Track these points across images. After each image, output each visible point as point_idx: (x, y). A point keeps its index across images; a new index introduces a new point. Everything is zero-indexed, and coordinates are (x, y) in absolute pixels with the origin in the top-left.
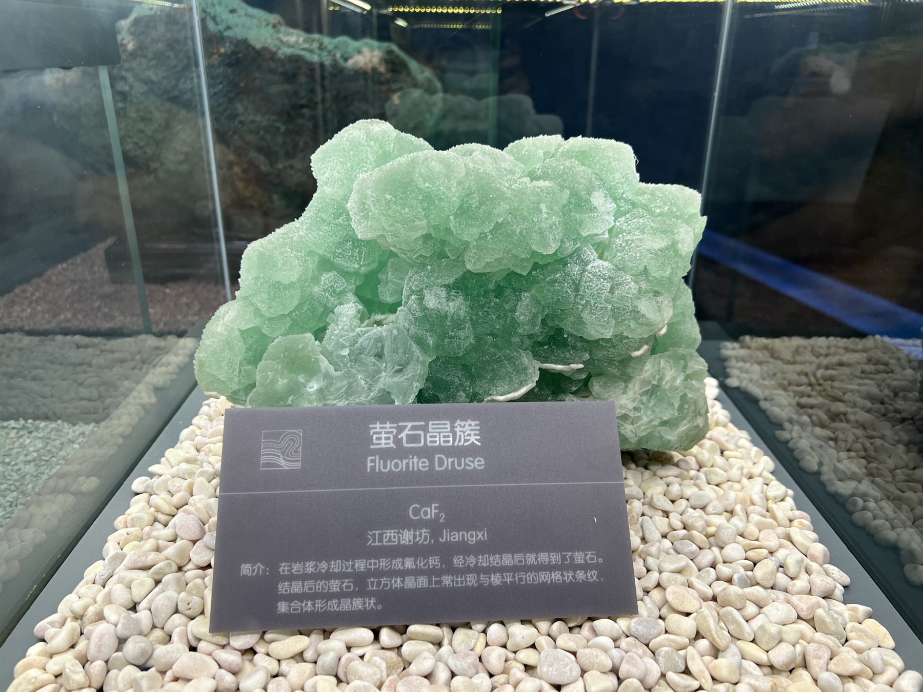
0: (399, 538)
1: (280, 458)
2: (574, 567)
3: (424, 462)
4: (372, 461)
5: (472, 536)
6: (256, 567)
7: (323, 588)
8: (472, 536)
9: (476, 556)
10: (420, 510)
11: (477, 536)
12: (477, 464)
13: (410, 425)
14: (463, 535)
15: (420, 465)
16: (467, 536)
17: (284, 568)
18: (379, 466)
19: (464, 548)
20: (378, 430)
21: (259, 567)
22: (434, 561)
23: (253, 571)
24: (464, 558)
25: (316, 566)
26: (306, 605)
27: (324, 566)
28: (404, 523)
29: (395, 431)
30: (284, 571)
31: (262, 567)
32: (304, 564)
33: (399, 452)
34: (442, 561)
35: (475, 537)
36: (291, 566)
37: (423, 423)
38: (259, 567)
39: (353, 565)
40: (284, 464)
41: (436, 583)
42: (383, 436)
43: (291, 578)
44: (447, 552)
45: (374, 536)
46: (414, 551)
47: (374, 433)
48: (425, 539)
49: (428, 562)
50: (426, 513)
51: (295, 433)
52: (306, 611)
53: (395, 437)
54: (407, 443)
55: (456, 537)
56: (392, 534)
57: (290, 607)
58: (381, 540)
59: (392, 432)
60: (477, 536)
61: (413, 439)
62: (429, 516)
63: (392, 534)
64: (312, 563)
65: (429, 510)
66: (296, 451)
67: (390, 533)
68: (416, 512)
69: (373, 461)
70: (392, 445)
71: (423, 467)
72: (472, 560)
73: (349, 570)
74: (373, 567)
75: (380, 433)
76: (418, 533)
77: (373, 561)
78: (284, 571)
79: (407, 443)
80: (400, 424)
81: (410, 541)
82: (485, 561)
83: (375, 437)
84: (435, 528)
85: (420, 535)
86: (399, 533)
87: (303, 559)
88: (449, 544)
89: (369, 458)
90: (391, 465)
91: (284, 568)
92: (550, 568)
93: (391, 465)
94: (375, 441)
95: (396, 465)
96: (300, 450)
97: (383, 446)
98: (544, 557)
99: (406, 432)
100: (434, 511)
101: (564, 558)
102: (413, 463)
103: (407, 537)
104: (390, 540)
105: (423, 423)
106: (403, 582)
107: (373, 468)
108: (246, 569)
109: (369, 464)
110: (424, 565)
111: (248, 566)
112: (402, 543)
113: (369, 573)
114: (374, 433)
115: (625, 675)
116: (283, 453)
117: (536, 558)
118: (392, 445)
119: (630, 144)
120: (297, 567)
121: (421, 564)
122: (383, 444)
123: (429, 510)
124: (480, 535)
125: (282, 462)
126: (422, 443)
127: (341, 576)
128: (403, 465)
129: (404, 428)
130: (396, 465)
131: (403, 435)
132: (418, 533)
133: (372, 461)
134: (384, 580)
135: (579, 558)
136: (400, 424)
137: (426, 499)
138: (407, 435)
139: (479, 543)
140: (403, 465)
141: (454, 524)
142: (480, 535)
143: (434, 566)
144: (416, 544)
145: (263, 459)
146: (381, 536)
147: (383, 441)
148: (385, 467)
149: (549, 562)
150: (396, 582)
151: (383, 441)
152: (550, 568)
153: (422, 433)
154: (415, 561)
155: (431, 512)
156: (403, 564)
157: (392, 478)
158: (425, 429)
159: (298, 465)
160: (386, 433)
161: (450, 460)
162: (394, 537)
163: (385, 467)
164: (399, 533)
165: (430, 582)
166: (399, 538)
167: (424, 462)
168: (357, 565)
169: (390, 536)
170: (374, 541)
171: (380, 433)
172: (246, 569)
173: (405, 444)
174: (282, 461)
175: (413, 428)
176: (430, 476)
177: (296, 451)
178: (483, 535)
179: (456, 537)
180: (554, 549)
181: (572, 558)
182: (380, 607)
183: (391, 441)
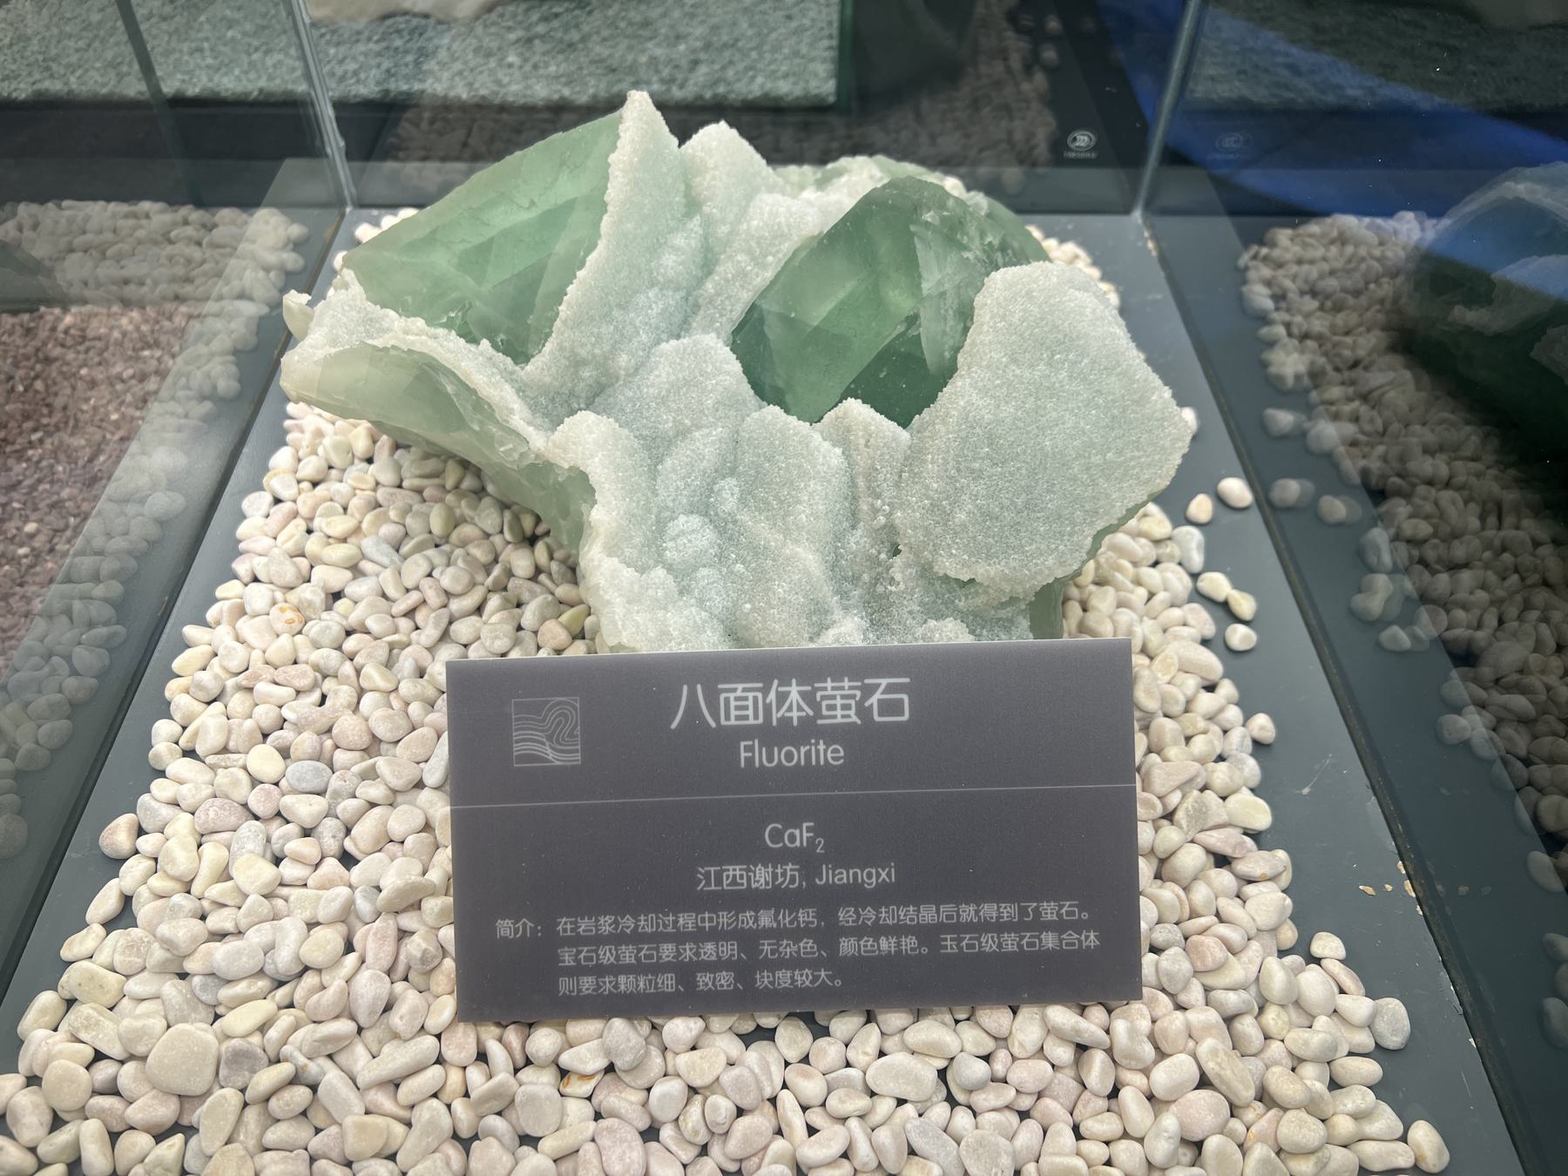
0: (749, 878)
1: (546, 747)
2: (1039, 926)
3: (836, 751)
4: (747, 749)
5: (870, 876)
8: (870, 876)
9: (797, 942)
11: (878, 875)
12: (828, 754)
13: (884, 682)
14: (855, 875)
15: (829, 755)
16: (862, 876)
17: (564, 925)
18: (760, 757)
19: (855, 895)
20: (829, 692)
21: (524, 925)
22: (806, 916)
24: (856, 912)
25: (616, 923)
26: (1087, 937)
27: (628, 922)
28: (754, 853)
29: (858, 693)
30: (565, 930)
32: (597, 921)
33: (773, 734)
34: (819, 916)
36: (575, 923)
38: (524, 925)
39: (676, 922)
40: (552, 756)
42: (839, 702)
44: (827, 901)
45: (707, 875)
46: (773, 898)
47: (823, 698)
48: (793, 880)
49: (796, 918)
50: (792, 838)
52: (1088, 947)
53: (860, 705)
54: (902, 714)
55: (843, 877)
57: (1061, 941)
58: (719, 882)
59: (853, 697)
60: (878, 875)
62: (798, 843)
64: (609, 919)
65: (797, 832)
66: (571, 735)
67: (733, 870)
68: (777, 836)
69: (749, 749)
70: (854, 719)
72: (869, 914)
73: (670, 930)
75: (834, 697)
76: (779, 871)
78: (565, 930)
79: (880, 715)
80: (867, 681)
81: (767, 883)
82: (887, 916)
83: (824, 703)
84: (807, 861)
85: (784, 874)
86: (748, 870)
87: (595, 911)
88: (829, 888)
89: (743, 744)
90: (779, 756)
91: (564, 925)
92: (999, 927)
93: (779, 756)
94: (825, 712)
95: (789, 756)
96: (578, 731)
97: (839, 720)
98: (989, 910)
99: (878, 696)
100: (805, 835)
101: (1023, 912)
102: (818, 751)
103: (762, 877)
104: (734, 882)
107: (750, 761)
108: (505, 928)
109: (743, 755)
110: (791, 922)
111: (508, 923)
112: (754, 886)
113: (941, 928)
114: (823, 698)
115: (690, 1148)
116: (550, 738)
117: (977, 912)
118: (854, 719)
120: (585, 925)
121: (786, 919)
122: (839, 717)
123: (797, 832)
124: (884, 875)
125: (551, 755)
126: (906, 717)
128: (799, 755)
129: (878, 685)
130: (789, 756)
131: (873, 700)
132: (779, 871)
133: (747, 749)
135: (1049, 911)
136: (867, 681)
138: (880, 701)
139: (882, 886)
140: (799, 755)
141: (840, 857)
142: (884, 875)
144: (776, 888)
145: (518, 749)
146: (719, 876)
147: (839, 712)
148: (770, 760)
149: (998, 918)
151: (839, 712)
152: (999, 927)
154: (776, 915)
155: (801, 835)
156: (756, 920)
159: (577, 758)
160: (843, 697)
161: (803, 750)
162: (741, 877)
163: (770, 760)
164: (748, 870)
166: (749, 878)
167: (836, 751)
168: (681, 921)
170: (708, 883)
171: (834, 697)
172: (505, 928)
173: (877, 718)
174: (549, 751)
175: (890, 689)
177: (571, 735)
178: (889, 875)
179: (843, 877)
180: (1010, 899)
181: (1036, 911)
183: (852, 712)
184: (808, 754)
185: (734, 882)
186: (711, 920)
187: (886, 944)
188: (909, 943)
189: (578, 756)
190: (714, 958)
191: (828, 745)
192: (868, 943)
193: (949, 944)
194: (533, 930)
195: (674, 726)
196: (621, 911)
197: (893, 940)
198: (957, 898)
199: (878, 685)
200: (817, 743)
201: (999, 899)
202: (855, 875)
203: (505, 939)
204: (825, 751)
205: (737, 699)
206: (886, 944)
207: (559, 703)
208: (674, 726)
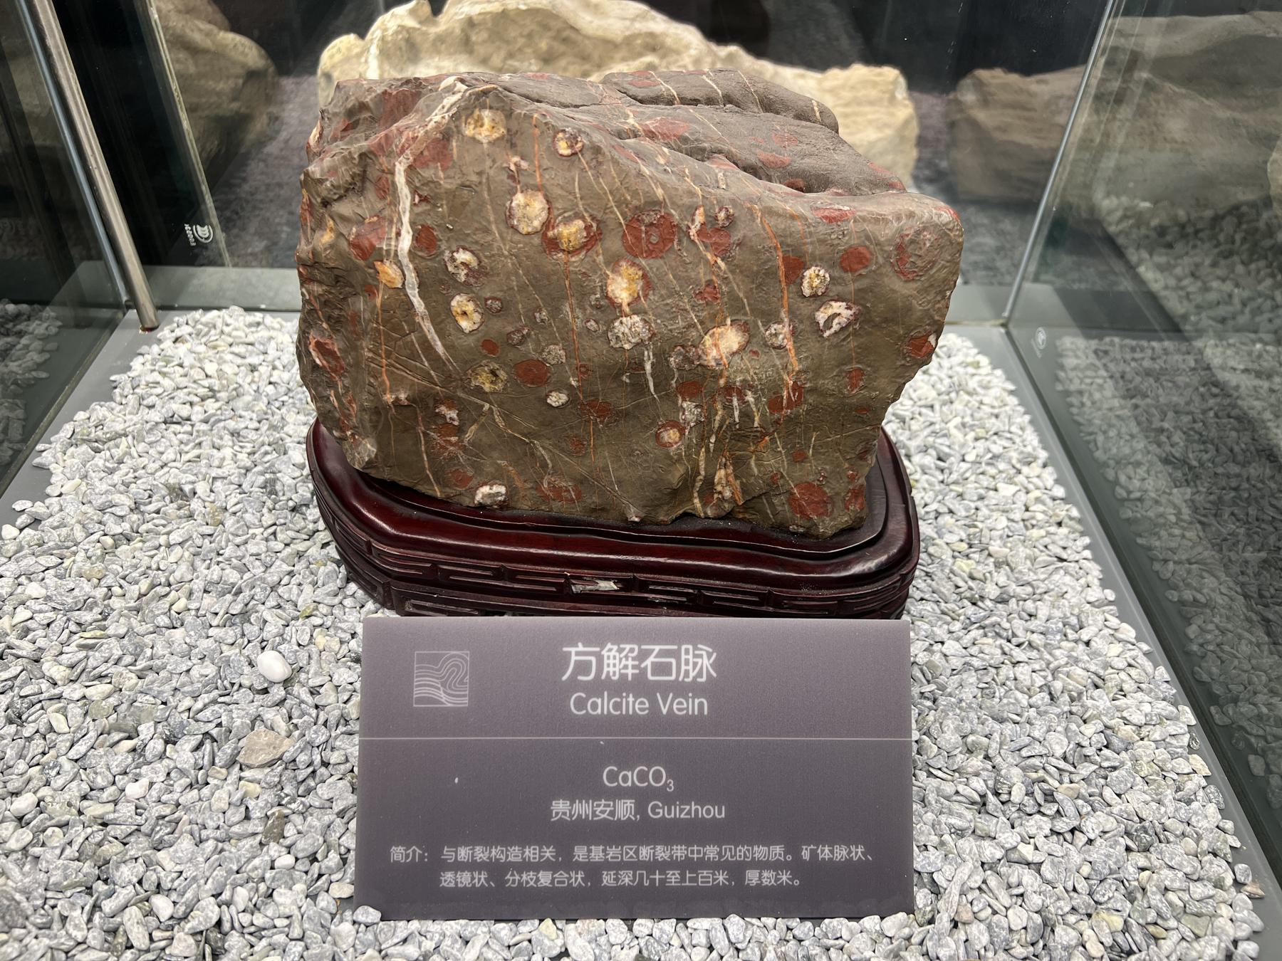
7: (745, 856)
9: (520, 873)
12: (694, 706)
13: (657, 648)
14: (669, 813)
15: (637, 706)
21: (414, 852)
23: (407, 856)
28: (596, 792)
31: (418, 851)
38: (414, 852)
40: (446, 700)
41: (691, 880)
43: (458, 866)
50: (625, 779)
51: (460, 657)
54: (670, 675)
61: (661, 669)
62: (629, 784)
65: (629, 774)
66: (462, 682)
68: (613, 777)
71: (641, 709)
79: (653, 674)
84: (642, 797)
96: (467, 680)
98: (531, 853)
99: (651, 659)
102: (627, 703)
106: (832, 852)
108: (398, 853)
111: (401, 849)
113: (607, 865)
116: (444, 685)
119: (347, 32)
125: (443, 697)
127: (715, 866)
131: (648, 663)
137: (626, 758)
138: (653, 663)
145: (417, 692)
150: (823, 851)
153: (673, 661)
156: (637, 852)
159: (464, 702)
165: (683, 879)
168: (844, 853)
172: (398, 853)
173: (650, 677)
174: (443, 695)
175: (662, 654)
176: (654, 721)
177: (462, 682)
186: (699, 852)
188: (721, 878)
189: (466, 700)
190: (452, 885)
191: (636, 697)
193: (608, 879)
194: (422, 857)
195: (564, 678)
196: (689, 843)
198: (506, 841)
200: (627, 696)
201: (767, 842)
202: (669, 813)
203: (397, 862)
204: (634, 703)
205: (578, 654)
208: (564, 678)
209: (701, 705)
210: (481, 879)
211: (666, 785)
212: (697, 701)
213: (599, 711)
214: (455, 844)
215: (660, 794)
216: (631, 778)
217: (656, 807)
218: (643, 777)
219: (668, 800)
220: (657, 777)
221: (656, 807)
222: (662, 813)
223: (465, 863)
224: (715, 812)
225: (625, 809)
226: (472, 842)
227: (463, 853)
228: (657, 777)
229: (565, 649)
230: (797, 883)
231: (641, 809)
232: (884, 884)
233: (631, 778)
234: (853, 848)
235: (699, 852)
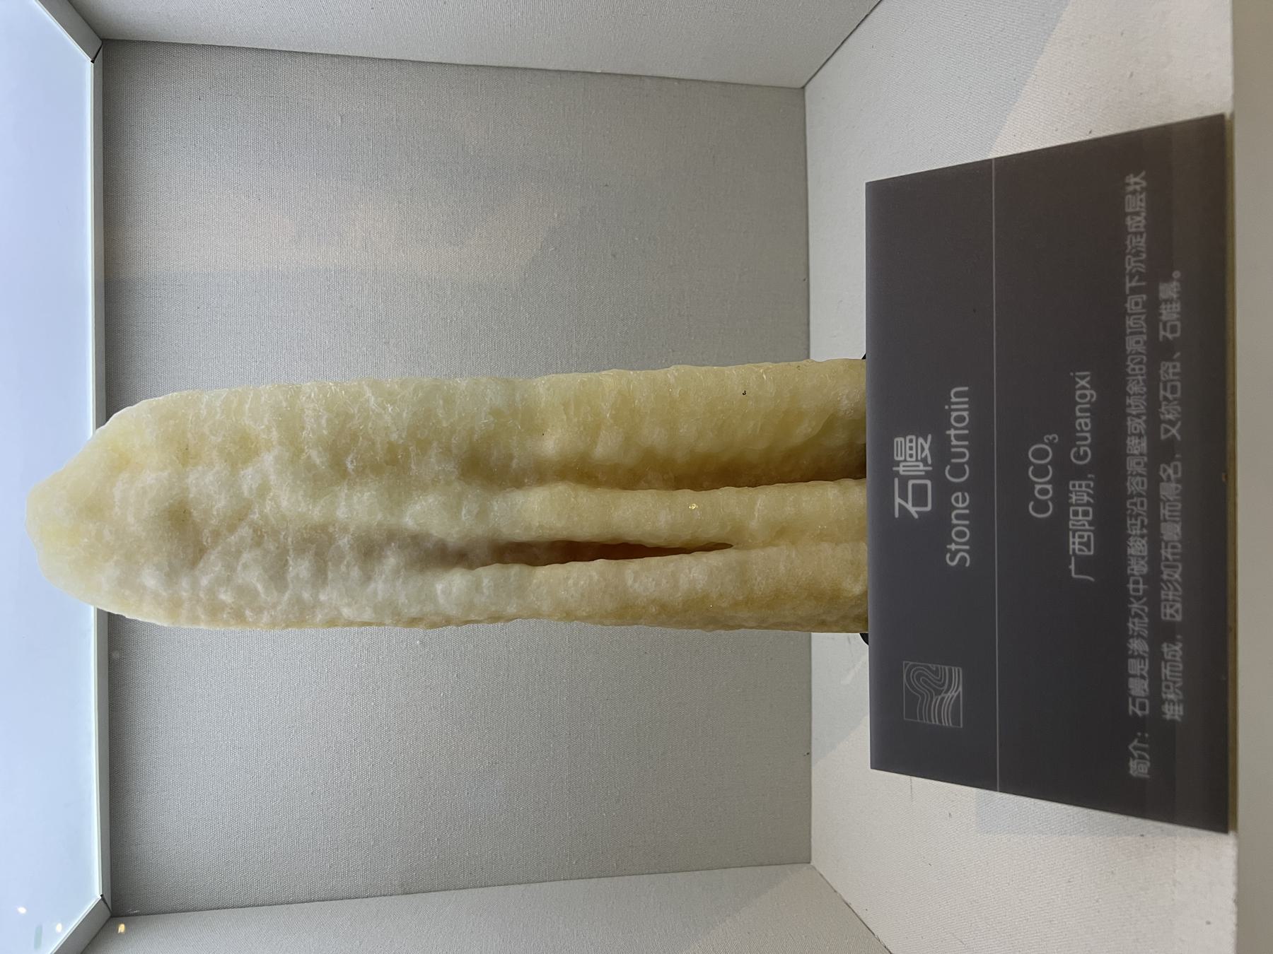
3: (957, 500)
5: (1083, 396)
6: (1135, 754)
10: (1037, 501)
13: (898, 500)
21: (1136, 748)
23: (1142, 757)
31: (1135, 743)
35: (1085, 390)
37: (896, 481)
38: (1136, 748)
40: (955, 692)
51: (908, 675)
56: (1077, 540)
60: (1083, 388)
62: (1049, 487)
63: (1077, 540)
65: (1038, 487)
66: (936, 673)
67: (1075, 544)
68: (1041, 506)
74: (1141, 586)
77: (1131, 586)
84: (1065, 473)
95: (961, 534)
99: (909, 506)
101: (1134, 291)
104: (1087, 545)
105: (896, 481)
108: (1139, 768)
113: (1152, 431)
116: (939, 693)
124: (1083, 383)
125: (952, 694)
129: (900, 505)
130: (961, 534)
131: (913, 510)
134: (1166, 553)
139: (1093, 385)
142: (1083, 383)
143: (1143, 526)
145: (947, 723)
153: (911, 482)
157: (979, 544)
158: (904, 480)
167: (957, 500)
169: (1080, 538)
173: (929, 508)
175: (904, 496)
176: (977, 487)
178: (1083, 378)
182: (1176, 274)
184: (958, 437)
185: (1087, 545)
187: (1169, 490)
189: (955, 670)
191: (952, 541)
192: (1168, 594)
194: (1142, 740)
197: (1141, 469)
199: (900, 505)
202: (1081, 410)
206: (1169, 490)
207: (908, 680)
209: (958, 395)
210: (1171, 471)
211: (1051, 444)
212: (954, 399)
213: (965, 414)
214: (1124, 692)
215: (1062, 451)
216: (1042, 486)
217: (1078, 457)
218: (1040, 471)
219: (1069, 437)
220: (1041, 454)
221: (1078, 457)
222: (1085, 448)
223: (1154, 680)
224: (1085, 390)
225: (1081, 493)
226: (1123, 676)
227: (1138, 687)
228: (1041, 454)
229: (897, 515)
230: (1179, 637)
231: (1080, 473)
232: (1188, 162)
233: (1042, 486)
234: (1130, 188)
235: (1136, 582)
